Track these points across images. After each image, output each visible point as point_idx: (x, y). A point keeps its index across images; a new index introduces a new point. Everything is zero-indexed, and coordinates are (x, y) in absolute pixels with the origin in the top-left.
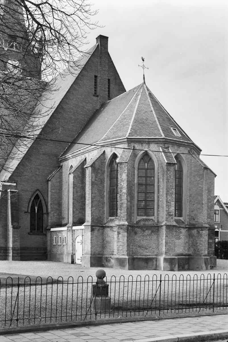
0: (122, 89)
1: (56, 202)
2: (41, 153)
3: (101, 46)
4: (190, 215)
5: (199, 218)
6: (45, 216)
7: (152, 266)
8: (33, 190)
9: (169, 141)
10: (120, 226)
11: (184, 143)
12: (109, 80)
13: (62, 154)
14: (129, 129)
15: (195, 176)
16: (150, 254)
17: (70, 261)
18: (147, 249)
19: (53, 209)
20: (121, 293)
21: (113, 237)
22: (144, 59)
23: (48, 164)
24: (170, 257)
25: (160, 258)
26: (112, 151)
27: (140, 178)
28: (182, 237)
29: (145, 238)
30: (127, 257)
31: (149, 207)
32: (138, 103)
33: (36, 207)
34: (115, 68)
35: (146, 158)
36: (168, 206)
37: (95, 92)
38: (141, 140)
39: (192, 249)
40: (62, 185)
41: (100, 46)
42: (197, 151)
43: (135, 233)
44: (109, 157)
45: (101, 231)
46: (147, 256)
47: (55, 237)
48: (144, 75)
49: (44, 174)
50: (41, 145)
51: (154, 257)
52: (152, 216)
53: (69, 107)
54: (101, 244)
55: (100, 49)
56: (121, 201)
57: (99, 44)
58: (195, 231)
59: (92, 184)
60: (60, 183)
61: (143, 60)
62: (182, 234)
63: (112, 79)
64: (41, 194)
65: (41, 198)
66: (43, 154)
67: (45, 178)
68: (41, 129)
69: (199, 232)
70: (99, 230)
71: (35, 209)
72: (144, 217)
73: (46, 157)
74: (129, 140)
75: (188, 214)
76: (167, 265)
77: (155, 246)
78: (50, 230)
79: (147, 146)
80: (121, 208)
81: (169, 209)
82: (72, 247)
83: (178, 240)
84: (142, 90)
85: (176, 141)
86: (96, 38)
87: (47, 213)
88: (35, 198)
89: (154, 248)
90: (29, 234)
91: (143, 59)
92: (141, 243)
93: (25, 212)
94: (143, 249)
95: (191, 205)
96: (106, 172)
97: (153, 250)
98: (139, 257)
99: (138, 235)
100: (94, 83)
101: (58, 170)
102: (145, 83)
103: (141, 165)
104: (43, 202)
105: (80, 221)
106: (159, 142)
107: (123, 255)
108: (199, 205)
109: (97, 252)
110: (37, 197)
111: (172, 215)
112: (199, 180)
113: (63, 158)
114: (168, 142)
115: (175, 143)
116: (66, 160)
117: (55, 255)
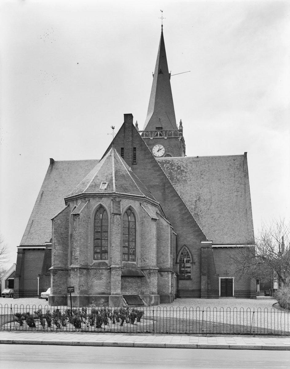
11: (105, 194)
20: (229, 319)
28: (103, 277)
35: (102, 210)
42: (128, 197)
62: (103, 275)
83: (99, 281)
115: (96, 196)
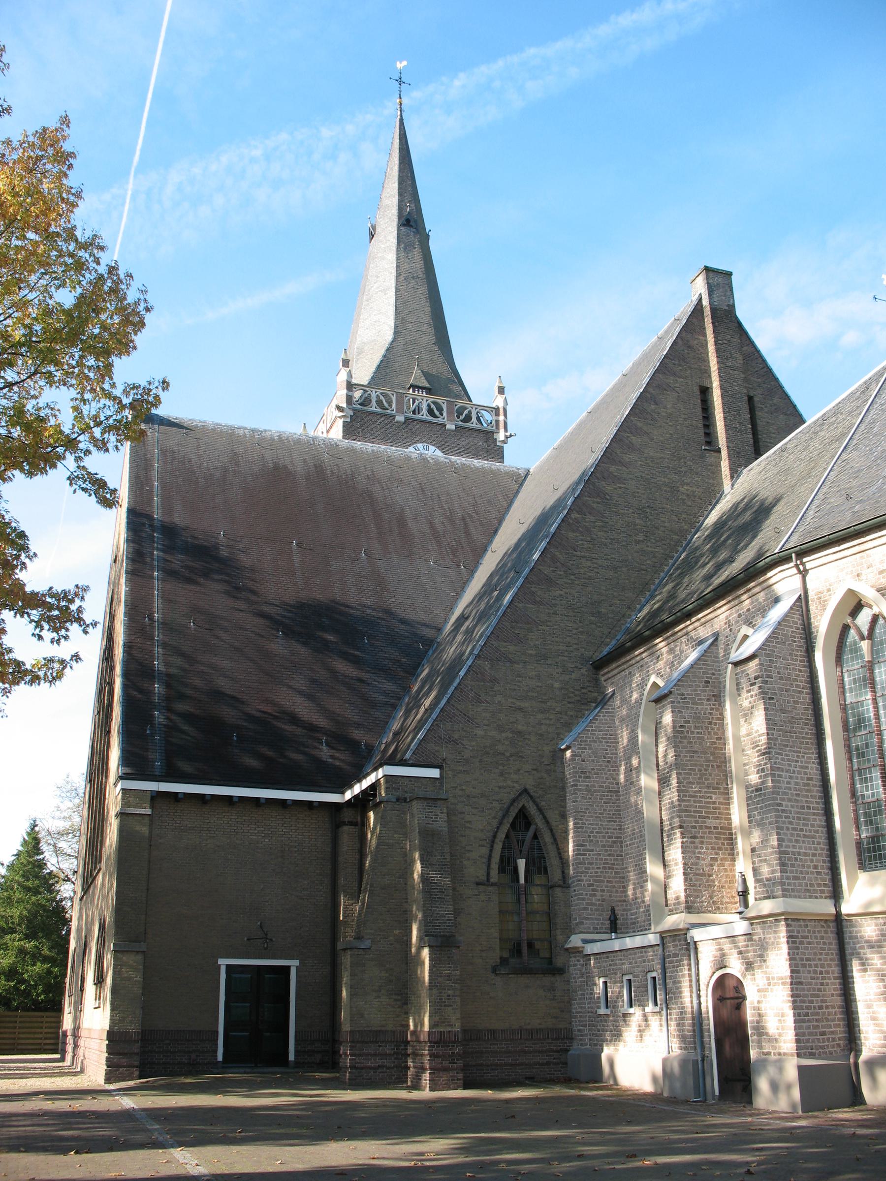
8: (507, 798)
42: (623, 664)
46: (733, 600)
53: (620, 488)
65: (539, 821)
88: (513, 825)
90: (495, 970)
100: (701, 432)
110: (522, 820)
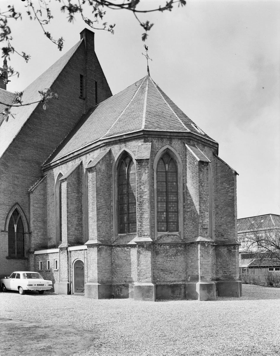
0: (109, 94)
1: (40, 219)
2: (20, 158)
3: (87, 42)
4: (217, 231)
5: (229, 234)
6: (27, 236)
7: (179, 295)
9: (194, 136)
10: (140, 245)
11: (209, 142)
12: (96, 83)
13: (45, 162)
14: (143, 121)
15: (223, 183)
16: (176, 279)
17: (66, 291)
18: (172, 273)
19: (37, 227)
21: (126, 260)
22: (147, 47)
23: (29, 173)
24: (207, 283)
25: (196, 285)
26: (121, 149)
27: (159, 183)
29: (169, 260)
30: (152, 285)
31: (172, 220)
32: (146, 95)
33: (15, 225)
34: (102, 70)
36: (202, 218)
37: (81, 95)
38: (161, 133)
39: (221, 271)
40: (46, 198)
41: (85, 41)
43: (156, 253)
44: (116, 159)
45: (108, 251)
47: (41, 261)
48: (148, 66)
49: (24, 185)
50: (19, 148)
51: (181, 283)
52: (175, 231)
53: (52, 106)
54: (108, 268)
55: (85, 44)
56: (141, 210)
57: (85, 39)
58: (225, 249)
59: (97, 190)
60: (44, 196)
61: (147, 49)
63: (99, 82)
64: (21, 208)
65: (22, 214)
66: (23, 160)
67: (25, 189)
68: (37, 104)
69: (231, 250)
70: (106, 250)
71: (14, 228)
72: (166, 233)
73: (26, 164)
74: (146, 133)
75: (214, 229)
76: (205, 293)
77: (182, 269)
78: (34, 253)
79: (168, 142)
80: (141, 219)
81: (203, 221)
82: (68, 273)
84: (147, 83)
85: (202, 138)
86: (81, 33)
87: (30, 233)
88: (13, 214)
89: (181, 272)
91: (146, 47)
92: (163, 266)
93: (2, 231)
94: (166, 273)
95: (218, 218)
96: (113, 176)
97: (180, 274)
98: (163, 283)
99: (160, 256)
101: (42, 180)
102: (149, 75)
103: (161, 166)
104: (24, 219)
105: (78, 240)
106: (183, 138)
107: (147, 282)
108: (229, 219)
109: (105, 278)
111: (207, 229)
112: (229, 188)
113: (48, 166)
114: (194, 138)
116: (51, 168)
117: (138, 288)
